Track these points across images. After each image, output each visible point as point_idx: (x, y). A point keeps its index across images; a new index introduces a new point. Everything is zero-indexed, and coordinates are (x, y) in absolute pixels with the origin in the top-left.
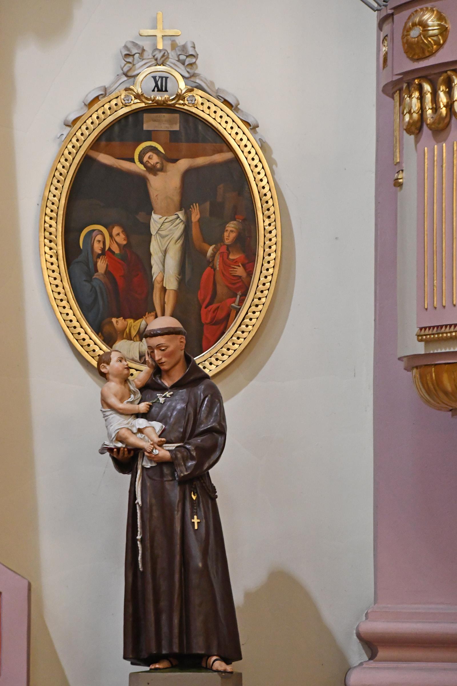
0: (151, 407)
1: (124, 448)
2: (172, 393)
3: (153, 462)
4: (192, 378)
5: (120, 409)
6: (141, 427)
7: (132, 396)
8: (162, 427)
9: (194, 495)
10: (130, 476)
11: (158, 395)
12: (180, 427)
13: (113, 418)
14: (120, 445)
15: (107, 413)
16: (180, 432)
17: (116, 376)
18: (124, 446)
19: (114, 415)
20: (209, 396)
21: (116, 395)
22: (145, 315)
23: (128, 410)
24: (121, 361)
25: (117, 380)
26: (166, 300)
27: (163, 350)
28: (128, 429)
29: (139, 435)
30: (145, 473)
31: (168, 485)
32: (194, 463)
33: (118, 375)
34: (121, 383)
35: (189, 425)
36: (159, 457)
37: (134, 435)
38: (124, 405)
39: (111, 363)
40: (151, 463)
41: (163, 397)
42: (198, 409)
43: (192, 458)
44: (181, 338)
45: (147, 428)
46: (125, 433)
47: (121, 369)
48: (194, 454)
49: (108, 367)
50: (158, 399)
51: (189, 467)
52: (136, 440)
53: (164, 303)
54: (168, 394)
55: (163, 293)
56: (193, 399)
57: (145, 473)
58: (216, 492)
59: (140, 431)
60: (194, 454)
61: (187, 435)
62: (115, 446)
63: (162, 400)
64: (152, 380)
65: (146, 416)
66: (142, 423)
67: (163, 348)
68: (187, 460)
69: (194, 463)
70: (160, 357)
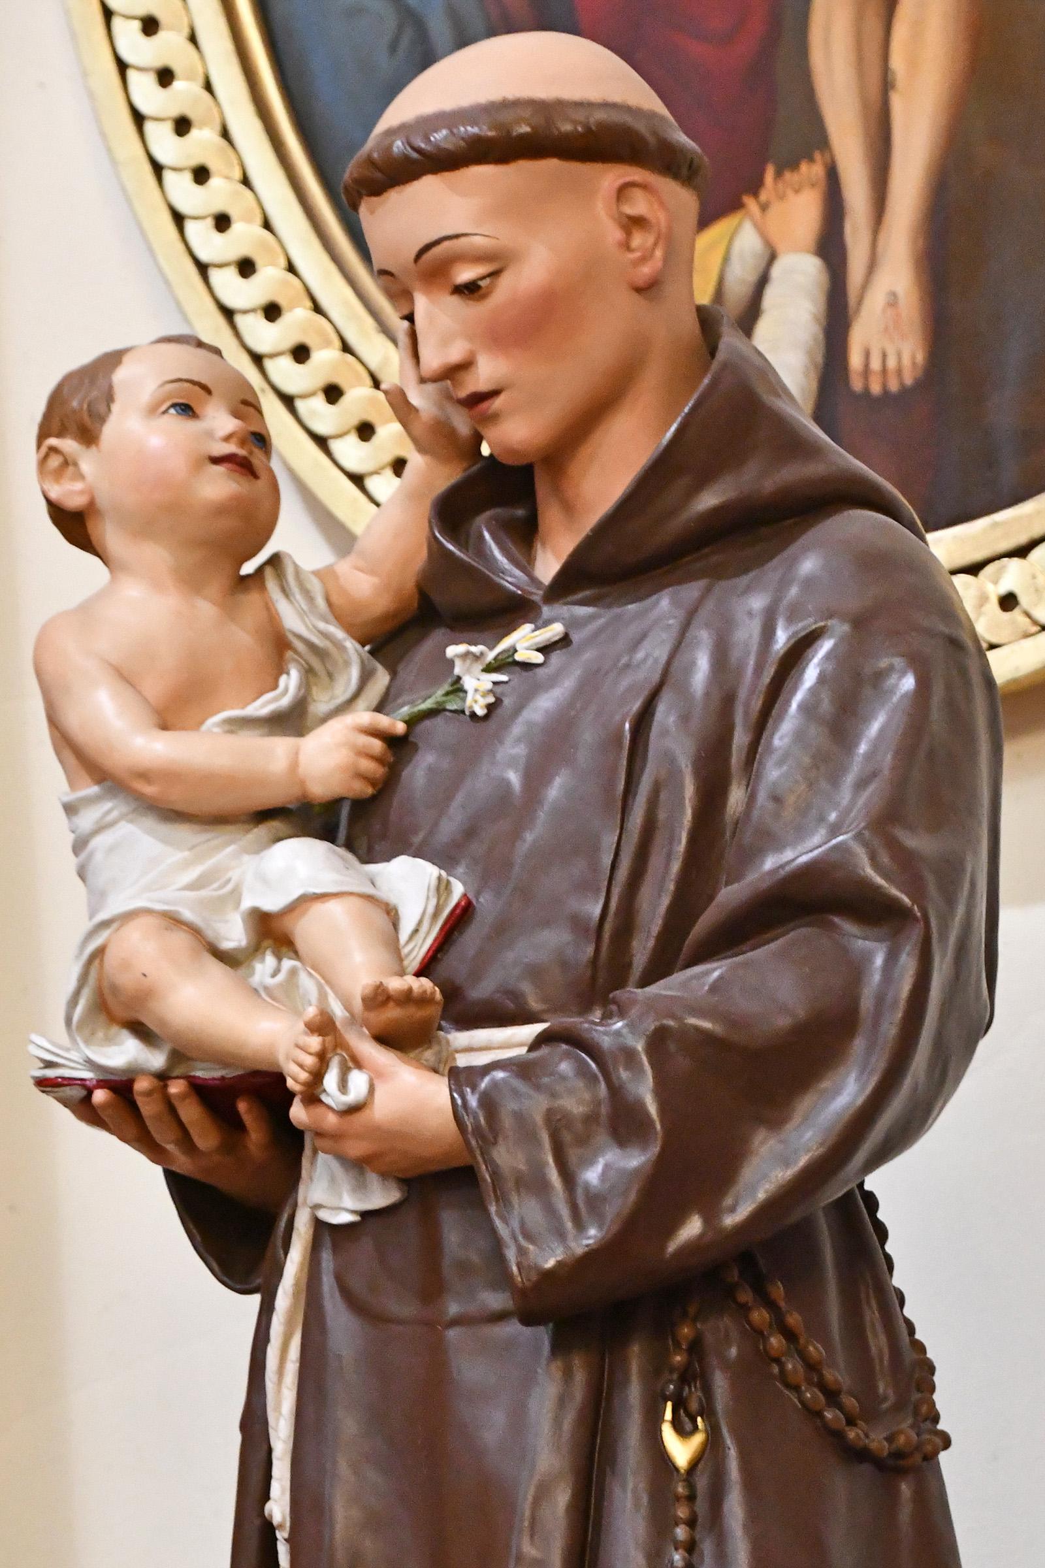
0: (398, 747)
1: (163, 1077)
2: (556, 630)
3: (373, 1178)
4: (708, 500)
5: (144, 775)
6: (272, 904)
7: (291, 681)
8: (443, 888)
9: (682, 1432)
10: (256, 1299)
11: (452, 651)
12: (584, 887)
13: (111, 849)
14: (123, 1052)
15: (87, 819)
16: (577, 923)
17: (144, 527)
18: (157, 1060)
19: (126, 829)
20: (840, 628)
21: (124, 677)
22: (755, 187)
23: (229, 781)
24: (187, 410)
25: (155, 556)
26: (897, 62)
27: (470, 290)
28: (173, 920)
29: (265, 968)
30: (327, 1259)
31: (471, 1368)
32: (635, 1160)
33: (162, 516)
34: (190, 581)
35: (655, 861)
36: (377, 1132)
37: (216, 969)
38: (208, 748)
39: (109, 432)
40: (360, 1187)
41: (489, 669)
42: (740, 738)
43: (624, 1123)
44: (622, 192)
45: (318, 908)
46: (143, 954)
47: (178, 465)
48: (644, 1090)
49: (88, 462)
50: (457, 689)
51: (595, 1200)
52: (260, 1024)
53: (887, 84)
54: (524, 640)
55: (873, 25)
56: (703, 664)
57: (327, 1259)
58: (936, 1418)
59: (272, 932)
60: (644, 1090)
61: (642, 950)
62: (91, 1064)
63: (478, 688)
64: (437, 553)
65: (356, 822)
66: (298, 866)
67: (465, 274)
68: (583, 1140)
69: (635, 1160)
70: (455, 353)
